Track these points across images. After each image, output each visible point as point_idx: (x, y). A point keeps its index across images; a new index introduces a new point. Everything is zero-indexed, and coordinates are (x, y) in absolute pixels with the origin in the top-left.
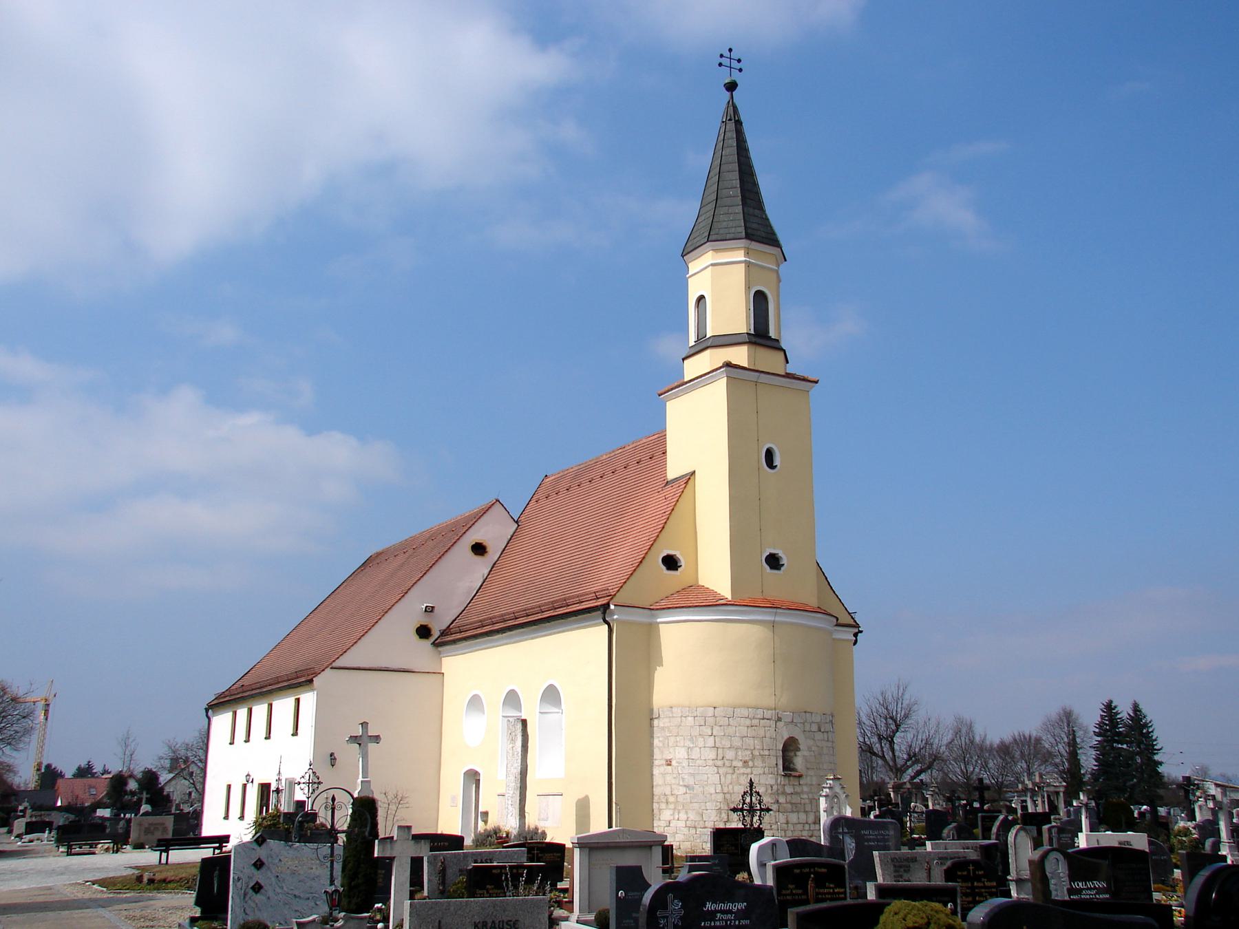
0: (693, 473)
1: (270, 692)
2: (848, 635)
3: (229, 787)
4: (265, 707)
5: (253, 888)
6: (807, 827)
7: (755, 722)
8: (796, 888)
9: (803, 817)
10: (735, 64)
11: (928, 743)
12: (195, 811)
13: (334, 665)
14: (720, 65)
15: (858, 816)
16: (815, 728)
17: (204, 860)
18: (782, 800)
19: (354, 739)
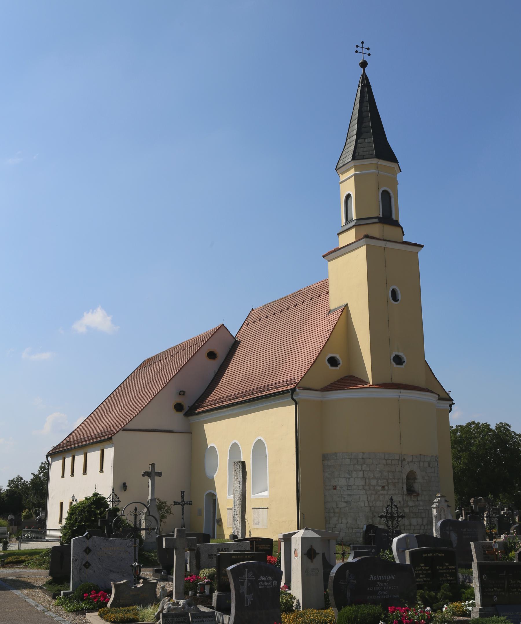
0: (347, 305)
1: (86, 446)
2: (445, 405)
3: (62, 504)
4: (82, 456)
5: (85, 565)
6: (423, 527)
7: (389, 462)
8: (425, 566)
9: (420, 521)
10: (366, 51)
12: (40, 519)
13: (127, 427)
14: (357, 52)
15: (455, 519)
16: (426, 465)
17: (53, 547)
19: (147, 474)
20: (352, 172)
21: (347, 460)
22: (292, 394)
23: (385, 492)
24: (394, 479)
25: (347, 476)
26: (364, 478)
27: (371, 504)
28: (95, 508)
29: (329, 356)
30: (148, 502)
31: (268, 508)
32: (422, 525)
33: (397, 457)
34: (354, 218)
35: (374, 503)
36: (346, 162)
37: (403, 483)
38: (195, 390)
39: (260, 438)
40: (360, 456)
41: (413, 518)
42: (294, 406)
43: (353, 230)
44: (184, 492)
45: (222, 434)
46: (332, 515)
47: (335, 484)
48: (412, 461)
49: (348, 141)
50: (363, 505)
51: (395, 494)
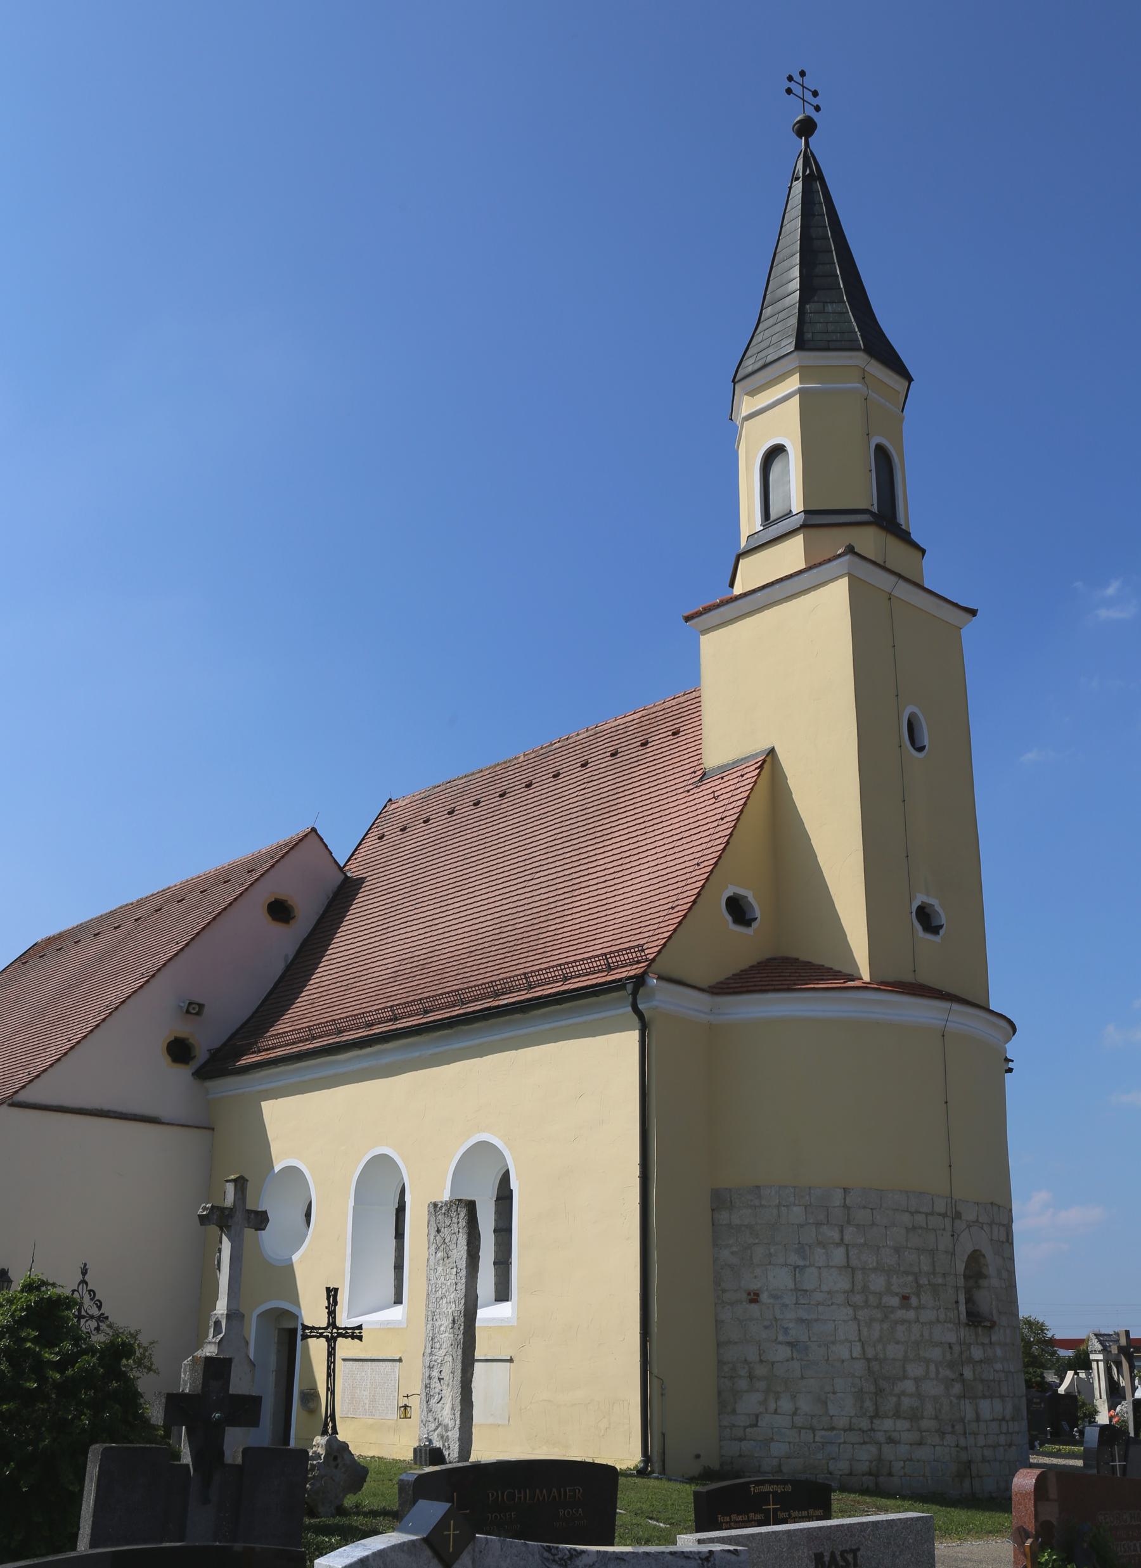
0: (772, 751)
7: (920, 1219)
11: (134, 1336)
13: (22, 1097)
18: (968, 1373)
20: (793, 383)
21: (795, 1209)
22: (635, 994)
23: (911, 1315)
24: (934, 1273)
25: (794, 1259)
26: (849, 1268)
27: (870, 1353)
28: (35, 1340)
29: (729, 892)
30: (217, 1324)
31: (511, 1360)
32: (1003, 1419)
33: (940, 1206)
34: (797, 505)
35: (879, 1347)
36: (770, 359)
37: (957, 1288)
38: (231, 1005)
39: (485, 1137)
40: (837, 1199)
41: (984, 1397)
42: (635, 1035)
43: (798, 541)
44: (336, 1290)
45: (321, 1135)
46: (743, 1384)
47: (754, 1286)
48: (977, 1221)
49: (768, 312)
50: (846, 1355)
51: (938, 1320)
